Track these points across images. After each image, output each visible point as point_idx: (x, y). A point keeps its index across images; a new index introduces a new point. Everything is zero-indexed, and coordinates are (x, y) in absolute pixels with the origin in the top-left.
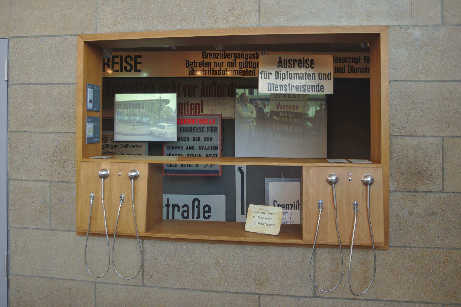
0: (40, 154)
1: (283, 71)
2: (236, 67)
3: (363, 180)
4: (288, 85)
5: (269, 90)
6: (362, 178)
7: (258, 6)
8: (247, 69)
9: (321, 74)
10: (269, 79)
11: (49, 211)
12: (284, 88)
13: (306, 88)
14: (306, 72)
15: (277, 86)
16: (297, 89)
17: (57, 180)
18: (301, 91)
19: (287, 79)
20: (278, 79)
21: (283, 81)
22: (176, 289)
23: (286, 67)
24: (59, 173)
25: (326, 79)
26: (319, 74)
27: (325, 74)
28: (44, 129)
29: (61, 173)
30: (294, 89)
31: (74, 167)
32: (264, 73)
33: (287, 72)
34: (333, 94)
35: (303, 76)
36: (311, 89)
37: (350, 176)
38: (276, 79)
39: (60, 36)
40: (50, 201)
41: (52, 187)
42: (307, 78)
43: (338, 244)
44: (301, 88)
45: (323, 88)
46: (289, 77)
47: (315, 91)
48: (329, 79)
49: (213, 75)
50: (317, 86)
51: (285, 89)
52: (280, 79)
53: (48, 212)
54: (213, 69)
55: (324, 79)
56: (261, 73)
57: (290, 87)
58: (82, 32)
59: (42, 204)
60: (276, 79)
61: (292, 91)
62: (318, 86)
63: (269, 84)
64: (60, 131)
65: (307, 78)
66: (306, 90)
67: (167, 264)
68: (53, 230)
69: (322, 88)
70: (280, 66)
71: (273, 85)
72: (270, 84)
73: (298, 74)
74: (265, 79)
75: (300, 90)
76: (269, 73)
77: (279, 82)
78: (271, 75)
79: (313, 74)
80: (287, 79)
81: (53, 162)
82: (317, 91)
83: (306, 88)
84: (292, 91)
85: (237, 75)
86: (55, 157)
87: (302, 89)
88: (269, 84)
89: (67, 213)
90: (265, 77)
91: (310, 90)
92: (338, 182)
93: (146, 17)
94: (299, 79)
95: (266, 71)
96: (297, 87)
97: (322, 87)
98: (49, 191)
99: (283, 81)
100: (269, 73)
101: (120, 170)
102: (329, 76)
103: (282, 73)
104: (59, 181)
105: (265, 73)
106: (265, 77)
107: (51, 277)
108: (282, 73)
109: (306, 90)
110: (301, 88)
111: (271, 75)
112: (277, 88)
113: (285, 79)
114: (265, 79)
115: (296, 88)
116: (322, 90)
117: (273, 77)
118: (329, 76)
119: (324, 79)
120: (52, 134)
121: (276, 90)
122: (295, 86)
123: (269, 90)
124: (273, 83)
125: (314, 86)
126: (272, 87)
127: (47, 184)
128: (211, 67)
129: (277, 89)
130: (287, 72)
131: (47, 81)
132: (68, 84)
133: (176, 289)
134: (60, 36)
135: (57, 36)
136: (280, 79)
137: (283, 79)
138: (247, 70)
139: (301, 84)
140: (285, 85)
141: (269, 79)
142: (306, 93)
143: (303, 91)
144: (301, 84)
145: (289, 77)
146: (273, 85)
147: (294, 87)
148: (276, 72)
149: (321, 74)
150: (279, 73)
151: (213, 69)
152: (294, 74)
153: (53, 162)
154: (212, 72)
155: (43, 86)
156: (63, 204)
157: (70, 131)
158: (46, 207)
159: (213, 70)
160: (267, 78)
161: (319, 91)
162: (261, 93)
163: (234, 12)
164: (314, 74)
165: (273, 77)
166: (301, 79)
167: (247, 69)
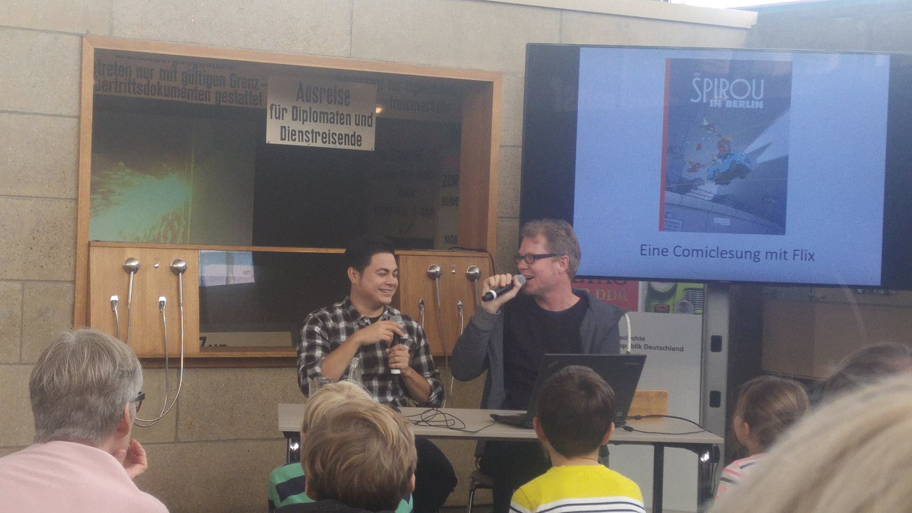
0: (7, 233)
1: (305, 106)
2: (175, 80)
3: (469, 274)
4: (310, 132)
5: (282, 139)
6: (467, 272)
7: (349, 26)
8: (196, 87)
9: (359, 115)
10: (283, 119)
11: (19, 331)
12: (305, 137)
13: (336, 138)
14: (337, 112)
15: (295, 131)
16: (324, 140)
17: (36, 278)
18: (329, 143)
19: (310, 121)
20: (296, 120)
21: (303, 124)
22: (224, 441)
23: (308, 101)
24: (42, 267)
25: (365, 125)
26: (356, 115)
27: (365, 116)
28: (15, 191)
29: (45, 267)
30: (319, 139)
31: (70, 257)
32: (276, 108)
33: (310, 108)
34: (374, 150)
35: (333, 118)
36: (343, 141)
37: (453, 268)
38: (293, 119)
39: (48, 32)
40: (22, 314)
41: (28, 291)
42: (339, 121)
43: (442, 355)
44: (329, 139)
45: (360, 141)
46: (313, 118)
47: (349, 145)
48: (369, 126)
49: (135, 93)
50: (352, 136)
51: (306, 138)
52: (300, 120)
53: (18, 333)
54: (134, 81)
55: (362, 125)
56: (271, 108)
57: (314, 135)
58: (88, 32)
59: (7, 321)
60: (293, 119)
61: (316, 142)
62: (353, 136)
63: (282, 127)
64: (46, 196)
65: (339, 121)
66: (337, 142)
67: (214, 404)
68: (25, 364)
69: (359, 140)
70: (300, 98)
71: (289, 130)
72: (285, 127)
73: (326, 113)
74: (276, 118)
75: (344, 143)
76: (283, 109)
77: (297, 126)
78: (286, 112)
79: (347, 115)
80: (310, 121)
81: (31, 248)
82: (352, 144)
83: (336, 138)
84: (316, 142)
85: (178, 97)
86: (34, 239)
87: (332, 139)
88: (282, 127)
89: (53, 333)
90: (277, 116)
91: (342, 142)
92: (32, 413)
93: (193, 20)
94: (327, 122)
95: (279, 106)
96: (324, 136)
97: (359, 138)
98: (21, 297)
99: (303, 124)
100: (283, 109)
101: (157, 260)
102: (370, 119)
103: (303, 110)
104: (41, 281)
105: (278, 107)
106: (277, 116)
107: (18, 445)
108: (303, 110)
109: (337, 142)
110: (329, 139)
111: (286, 112)
112: (295, 135)
113: (306, 120)
114: (276, 118)
115: (323, 138)
116: (359, 143)
117: (288, 116)
118: (370, 119)
119: (362, 125)
120: (31, 200)
121: (292, 140)
122: (337, 135)
123: (282, 139)
124: (289, 127)
125: (348, 135)
126: (287, 134)
127: (18, 286)
128: (130, 77)
129: (294, 137)
130: (310, 108)
131: (22, 108)
132: (61, 116)
133: (224, 441)
134: (48, 32)
135: (42, 31)
136: (300, 120)
137: (304, 121)
138: (196, 90)
139: (329, 131)
140: (307, 132)
141: (283, 119)
142: (337, 147)
143: (307, 141)
144: (329, 131)
145: (313, 118)
146: (289, 130)
147: (319, 136)
148: (294, 107)
149: (359, 115)
150: (299, 111)
151: (134, 81)
152: (321, 113)
153: (31, 248)
154: (132, 86)
155: (14, 116)
156: (46, 319)
157: (64, 196)
158: (14, 325)
159: (134, 84)
160: (279, 118)
161: (354, 144)
162: (270, 143)
163: (318, 31)
164: (350, 115)
165: (288, 116)
166: (331, 123)
167: (196, 87)
